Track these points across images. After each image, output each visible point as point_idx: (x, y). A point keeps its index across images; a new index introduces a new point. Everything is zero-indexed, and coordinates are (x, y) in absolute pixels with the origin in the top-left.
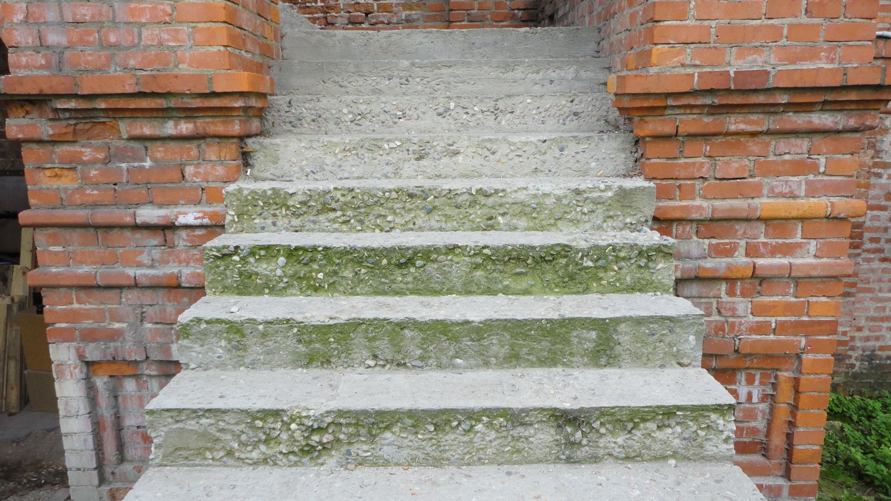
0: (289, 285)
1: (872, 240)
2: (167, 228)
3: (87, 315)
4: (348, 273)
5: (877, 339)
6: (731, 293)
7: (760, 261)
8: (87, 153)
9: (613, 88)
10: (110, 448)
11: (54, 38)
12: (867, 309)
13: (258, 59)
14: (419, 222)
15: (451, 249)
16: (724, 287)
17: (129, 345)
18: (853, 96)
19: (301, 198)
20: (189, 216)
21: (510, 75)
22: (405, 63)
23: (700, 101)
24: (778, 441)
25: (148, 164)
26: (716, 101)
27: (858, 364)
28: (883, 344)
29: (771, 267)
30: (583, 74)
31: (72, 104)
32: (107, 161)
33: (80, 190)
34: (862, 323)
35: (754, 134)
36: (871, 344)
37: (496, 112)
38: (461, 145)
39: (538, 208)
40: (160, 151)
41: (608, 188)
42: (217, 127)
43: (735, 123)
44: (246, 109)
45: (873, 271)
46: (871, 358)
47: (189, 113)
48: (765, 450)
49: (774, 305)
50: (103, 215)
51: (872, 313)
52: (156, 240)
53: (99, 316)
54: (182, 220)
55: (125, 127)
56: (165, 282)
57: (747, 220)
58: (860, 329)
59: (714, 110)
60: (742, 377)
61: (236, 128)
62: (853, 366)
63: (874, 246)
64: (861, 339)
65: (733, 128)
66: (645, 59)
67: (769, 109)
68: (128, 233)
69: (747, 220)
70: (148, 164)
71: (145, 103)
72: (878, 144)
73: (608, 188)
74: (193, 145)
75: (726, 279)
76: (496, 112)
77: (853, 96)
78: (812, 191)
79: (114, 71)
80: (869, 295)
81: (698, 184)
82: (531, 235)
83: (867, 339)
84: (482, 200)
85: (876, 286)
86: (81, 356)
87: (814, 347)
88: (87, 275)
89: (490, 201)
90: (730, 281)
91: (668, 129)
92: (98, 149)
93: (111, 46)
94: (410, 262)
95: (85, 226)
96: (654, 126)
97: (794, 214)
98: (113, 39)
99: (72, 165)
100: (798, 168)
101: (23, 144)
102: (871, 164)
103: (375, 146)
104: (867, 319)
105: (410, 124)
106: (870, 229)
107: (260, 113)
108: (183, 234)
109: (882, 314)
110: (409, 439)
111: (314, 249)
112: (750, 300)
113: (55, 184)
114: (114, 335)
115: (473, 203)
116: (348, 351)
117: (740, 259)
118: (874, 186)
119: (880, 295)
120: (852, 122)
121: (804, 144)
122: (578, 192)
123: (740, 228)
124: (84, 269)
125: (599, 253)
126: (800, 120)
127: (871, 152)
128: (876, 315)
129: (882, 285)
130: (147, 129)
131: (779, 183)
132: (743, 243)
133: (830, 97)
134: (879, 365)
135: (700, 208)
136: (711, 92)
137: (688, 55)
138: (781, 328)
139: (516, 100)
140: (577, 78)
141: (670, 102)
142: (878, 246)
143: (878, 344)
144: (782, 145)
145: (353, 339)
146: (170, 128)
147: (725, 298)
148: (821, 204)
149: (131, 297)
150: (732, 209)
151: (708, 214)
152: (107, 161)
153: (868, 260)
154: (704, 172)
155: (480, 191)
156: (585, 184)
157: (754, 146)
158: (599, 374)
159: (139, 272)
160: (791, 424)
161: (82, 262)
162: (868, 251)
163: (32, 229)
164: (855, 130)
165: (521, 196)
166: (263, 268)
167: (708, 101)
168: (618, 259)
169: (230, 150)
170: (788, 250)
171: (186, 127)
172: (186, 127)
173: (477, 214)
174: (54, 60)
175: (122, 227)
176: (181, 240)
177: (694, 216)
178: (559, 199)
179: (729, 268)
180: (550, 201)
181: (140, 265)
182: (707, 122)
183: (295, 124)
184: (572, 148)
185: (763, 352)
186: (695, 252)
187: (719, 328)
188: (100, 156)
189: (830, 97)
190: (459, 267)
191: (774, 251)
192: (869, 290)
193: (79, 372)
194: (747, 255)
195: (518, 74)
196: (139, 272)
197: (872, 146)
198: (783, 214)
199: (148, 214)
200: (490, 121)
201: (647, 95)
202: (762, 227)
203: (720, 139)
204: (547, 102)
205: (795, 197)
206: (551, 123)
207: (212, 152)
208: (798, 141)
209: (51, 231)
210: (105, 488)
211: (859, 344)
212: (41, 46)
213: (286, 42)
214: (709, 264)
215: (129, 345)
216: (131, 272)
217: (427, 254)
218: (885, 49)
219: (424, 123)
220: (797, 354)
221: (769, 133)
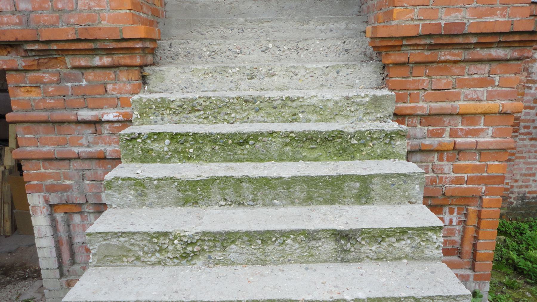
0: (172, 157)
1: (525, 127)
2: (97, 123)
3: (49, 176)
4: (208, 149)
6: (440, 159)
7: (458, 140)
8: (47, 77)
9: (369, 34)
10: (66, 256)
12: (521, 169)
13: (151, 18)
14: (251, 117)
15: (271, 134)
16: (436, 156)
17: (76, 194)
18: (517, 38)
19: (178, 103)
20: (110, 115)
21: (306, 27)
22: (242, 20)
23: (423, 42)
24: (467, 248)
25: (84, 83)
26: (433, 42)
27: (515, 202)
29: (465, 143)
30: (351, 26)
31: (36, 47)
32: (59, 82)
33: (43, 99)
34: (518, 177)
35: (455, 62)
36: (523, 190)
37: (297, 49)
38: (276, 70)
39: (324, 108)
40: (91, 75)
41: (366, 96)
42: (126, 60)
43: (444, 55)
44: (143, 49)
45: (525, 146)
46: (523, 198)
47: (108, 52)
48: (460, 253)
49: (467, 166)
50: (57, 115)
51: (524, 172)
52: (90, 130)
53: (57, 177)
54: (106, 118)
55: (69, 61)
56: (96, 156)
57: (451, 115)
60: (446, 210)
61: (138, 61)
62: (512, 203)
64: (517, 187)
65: (443, 58)
66: (389, 15)
67: (465, 46)
68: (73, 126)
69: (451, 115)
70: (84, 83)
71: (81, 46)
72: (530, 69)
73: (366, 96)
74: (111, 71)
75: (438, 151)
76: (297, 49)
77: (517, 38)
78: (491, 97)
79: (61, 26)
80: (522, 160)
81: (421, 93)
83: (521, 187)
84: (290, 104)
85: (527, 155)
86: (47, 201)
87: (490, 192)
88: (48, 152)
89: (294, 104)
90: (440, 152)
92: (53, 74)
93: (59, 10)
94: (246, 141)
96: (394, 57)
97: (479, 111)
98: (60, 6)
99: (37, 84)
100: (483, 83)
101: (7, 72)
102: (525, 81)
103: (223, 71)
105: (244, 57)
106: (524, 121)
107: (152, 51)
108: (107, 126)
109: (530, 172)
110: (246, 249)
111: (187, 134)
113: (27, 96)
114: (67, 188)
115: (284, 106)
116: (209, 196)
117: (446, 139)
118: (527, 94)
119: (529, 160)
120: (516, 54)
121: (486, 68)
122: (348, 98)
123: (447, 119)
124: (47, 148)
125: (361, 135)
126: (483, 53)
127: (525, 74)
128: (527, 172)
129: (531, 154)
130: (83, 62)
131: (471, 92)
132: (448, 129)
133: (502, 39)
134: (528, 202)
135: (422, 107)
136: (430, 36)
138: (470, 181)
139: (310, 42)
140: (347, 28)
141: (404, 42)
143: (527, 190)
144: (473, 69)
146: (97, 61)
147: (437, 162)
148: (496, 105)
149: (76, 165)
150: (442, 108)
151: (427, 111)
152: (59, 82)
153: (523, 140)
154: (425, 86)
155: (288, 98)
156: (352, 93)
157: (455, 69)
159: (81, 150)
160: (476, 238)
161: (45, 144)
162: (522, 134)
164: (517, 59)
165: (313, 101)
166: (156, 146)
167: (428, 41)
168: (372, 139)
169: (135, 74)
170: (475, 133)
171: (106, 61)
172: (106, 61)
173: (286, 112)
174: (24, 19)
175: (70, 122)
176: (106, 130)
177: (419, 112)
178: (336, 102)
179: (440, 144)
181: (81, 145)
183: (174, 58)
184: (344, 71)
186: (419, 135)
188: (55, 79)
189: (502, 39)
190: (275, 145)
191: (467, 134)
192: (523, 158)
193: (46, 211)
194: (451, 136)
195: (311, 26)
196: (81, 150)
197: (526, 70)
198: (473, 111)
199: (85, 114)
200: (294, 55)
201: (390, 38)
202: (460, 119)
203: (435, 65)
204: (329, 43)
205: (480, 101)
206: (331, 56)
207: (123, 75)
208: (483, 66)
209: (26, 125)
210: (64, 280)
211: (516, 190)
214: (427, 142)
215: (76, 194)
216: (76, 150)
217: (256, 136)
221: (464, 61)
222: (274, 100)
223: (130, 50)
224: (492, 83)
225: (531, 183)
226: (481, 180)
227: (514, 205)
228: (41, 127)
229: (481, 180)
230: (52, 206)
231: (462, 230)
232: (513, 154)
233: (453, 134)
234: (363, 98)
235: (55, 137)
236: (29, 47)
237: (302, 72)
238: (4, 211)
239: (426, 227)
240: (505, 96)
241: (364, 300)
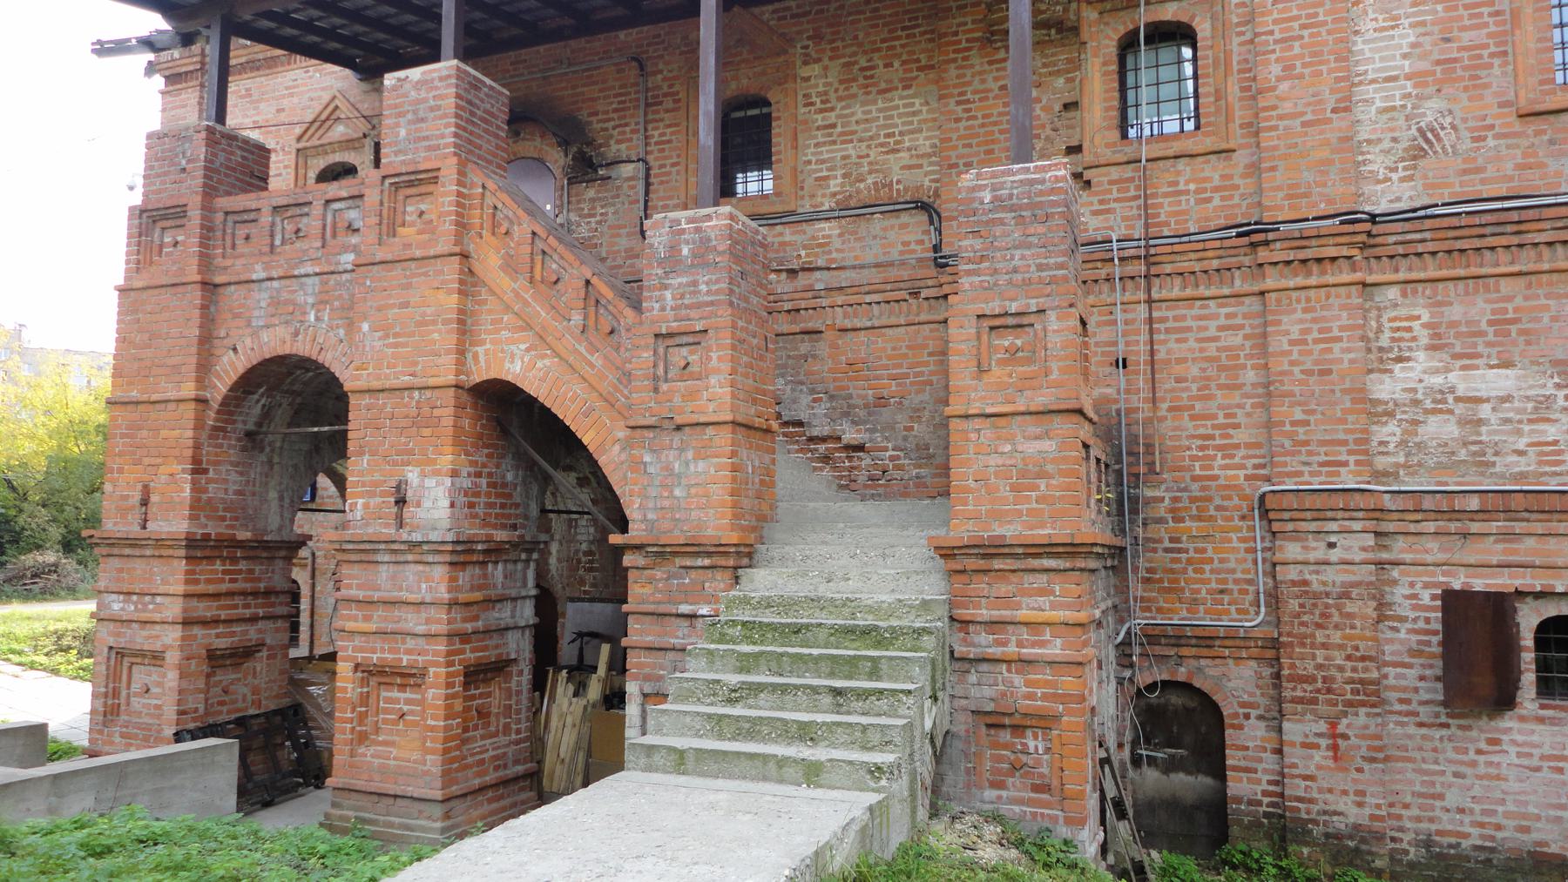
1: (1401, 701)
2: (692, 616)
5: (1431, 820)
6: (1009, 671)
8: (659, 574)
11: (651, 516)
12: (1411, 783)
13: (754, 523)
16: (1004, 666)
18: (1061, 550)
20: (704, 610)
27: (1412, 850)
28: (1440, 827)
32: (668, 579)
34: (1408, 799)
36: (1424, 826)
37: (884, 556)
39: (879, 609)
40: (693, 574)
42: (722, 561)
43: (997, 564)
44: (738, 553)
45: (1410, 737)
47: (709, 554)
49: (1038, 681)
50: (662, 609)
51: (1418, 788)
52: (686, 623)
53: (653, 666)
55: (679, 561)
58: (1406, 806)
59: (985, 556)
60: (1029, 733)
61: (731, 563)
62: (1406, 852)
63: (1404, 707)
64: (1410, 818)
74: (709, 572)
76: (884, 556)
77: (1061, 550)
78: (1053, 607)
79: (677, 533)
80: (1410, 765)
83: (1418, 819)
85: (1417, 755)
87: (1070, 713)
90: (1009, 662)
91: (959, 567)
95: (652, 614)
100: (1042, 592)
104: (1413, 794)
106: (1394, 688)
107: (750, 555)
109: (1432, 791)
110: (772, 698)
116: (758, 666)
117: (1012, 649)
118: (1391, 641)
119: (1425, 766)
121: (1044, 577)
123: (1010, 628)
124: (649, 638)
125: (892, 629)
128: (1424, 790)
129: (1425, 754)
130: (688, 563)
137: (970, 525)
138: (1045, 697)
142: (1410, 708)
143: (1434, 827)
144: (1028, 578)
146: (700, 562)
147: (1006, 674)
152: (668, 579)
153: (1402, 724)
154: (985, 593)
157: (1014, 578)
162: (1400, 713)
165: (869, 602)
166: (730, 631)
169: (729, 573)
170: (1042, 644)
171: (707, 562)
172: (707, 562)
173: (846, 611)
176: (699, 623)
180: (885, 606)
182: (982, 564)
183: (770, 561)
186: (984, 643)
187: (1004, 694)
190: (822, 635)
191: (1034, 644)
192: (1409, 760)
193: (639, 700)
195: (911, 532)
199: (685, 609)
206: (917, 563)
207: (719, 575)
211: (1408, 825)
212: (645, 520)
213: (779, 511)
217: (807, 627)
219: (841, 562)
223: (726, 553)
224: (1052, 593)
225: (1438, 813)
226: (1055, 697)
227: (1411, 856)
229: (1055, 697)
230: (645, 696)
232: (1380, 749)
233: (1020, 644)
235: (657, 628)
236: (650, 549)
237: (875, 577)
240: (1068, 607)
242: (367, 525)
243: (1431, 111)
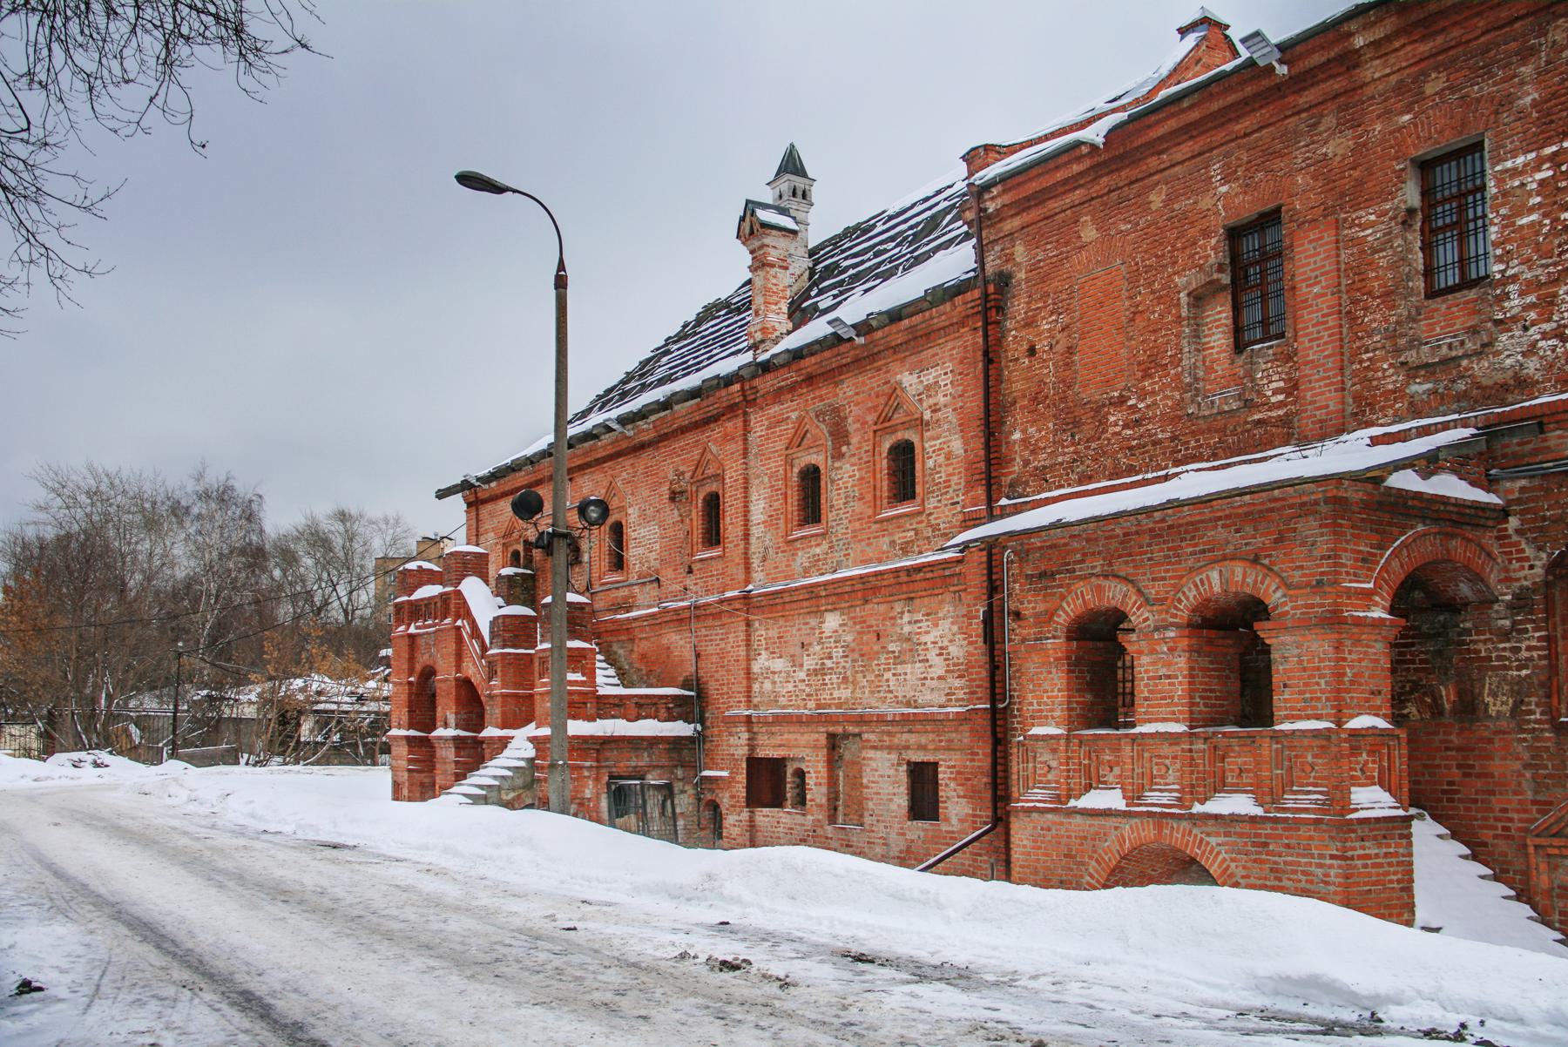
82: (31, 1012)
101: (1353, 789)
112: (1534, 872)
145: (953, 623)
158: (924, 830)
163: (1227, 32)
172: (1545, 465)
185: (82, 878)
190: (1452, 424)
192: (1329, 328)
218: (4, 321)
220: (1284, 333)
222: (61, 972)
228: (1211, 822)
231: (1228, 261)
234: (323, 744)
238: (1271, 457)
239: (1240, 815)
241: (174, 755)
242: (1214, 733)
243: (1296, 345)
